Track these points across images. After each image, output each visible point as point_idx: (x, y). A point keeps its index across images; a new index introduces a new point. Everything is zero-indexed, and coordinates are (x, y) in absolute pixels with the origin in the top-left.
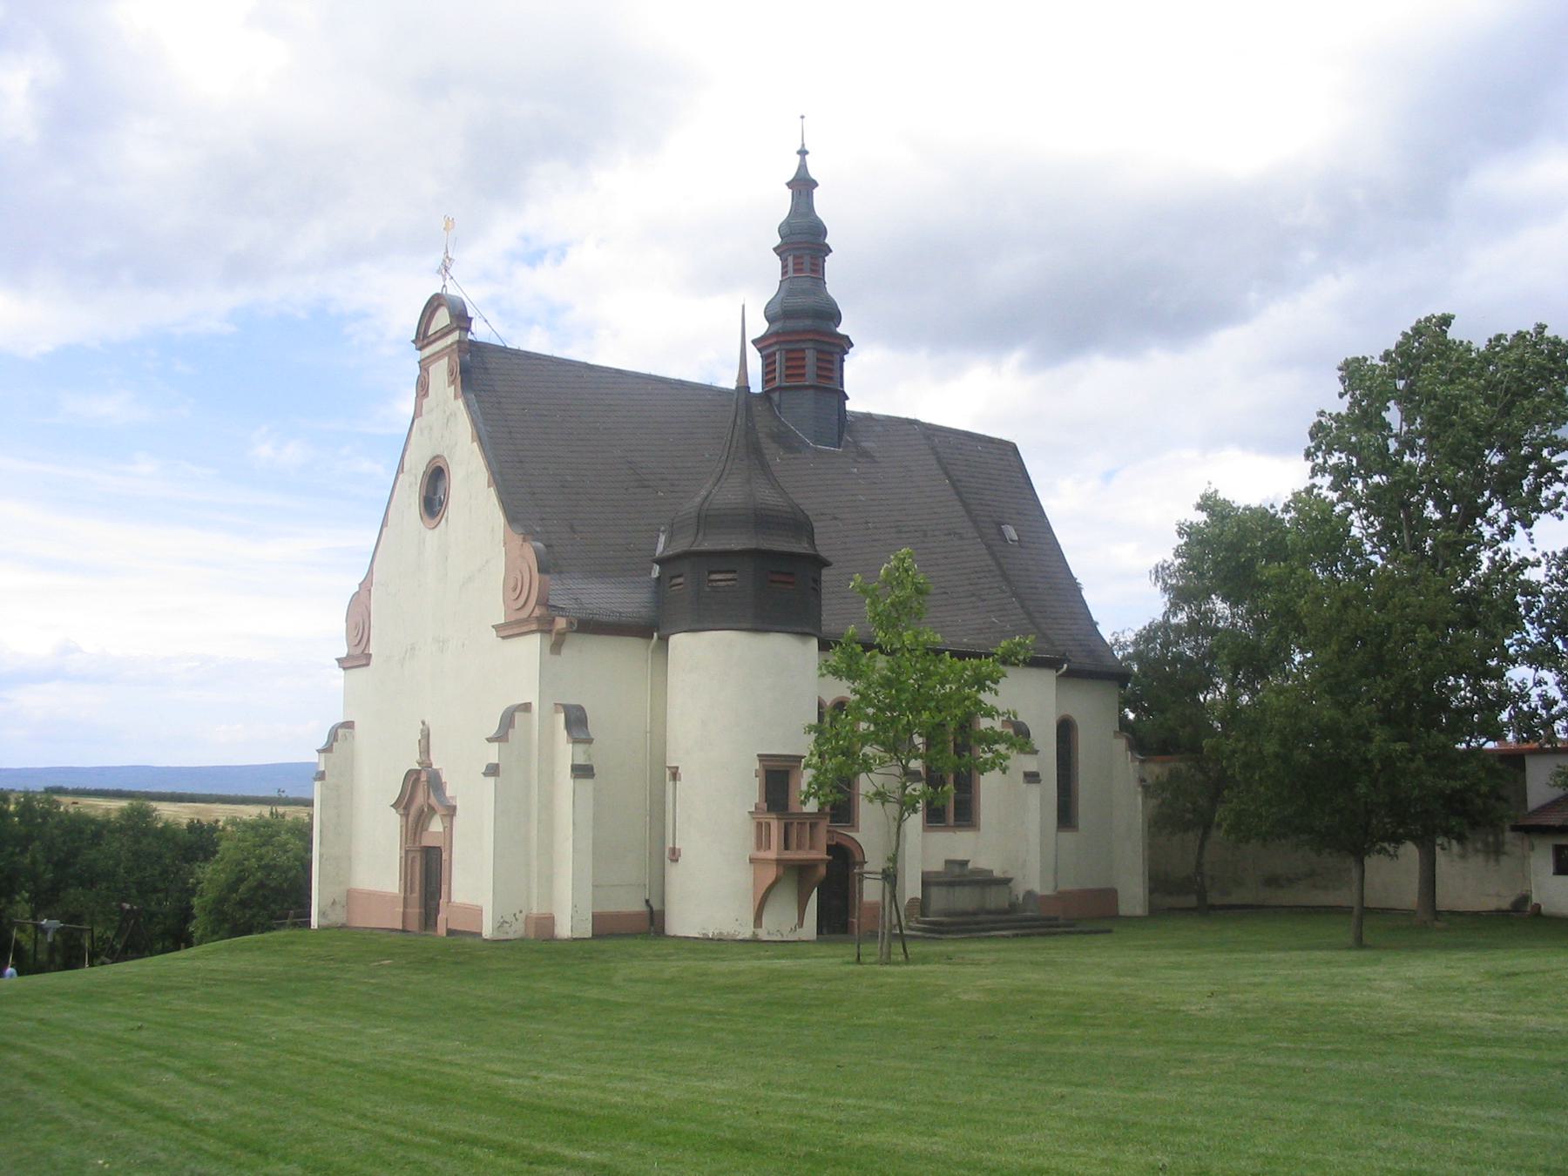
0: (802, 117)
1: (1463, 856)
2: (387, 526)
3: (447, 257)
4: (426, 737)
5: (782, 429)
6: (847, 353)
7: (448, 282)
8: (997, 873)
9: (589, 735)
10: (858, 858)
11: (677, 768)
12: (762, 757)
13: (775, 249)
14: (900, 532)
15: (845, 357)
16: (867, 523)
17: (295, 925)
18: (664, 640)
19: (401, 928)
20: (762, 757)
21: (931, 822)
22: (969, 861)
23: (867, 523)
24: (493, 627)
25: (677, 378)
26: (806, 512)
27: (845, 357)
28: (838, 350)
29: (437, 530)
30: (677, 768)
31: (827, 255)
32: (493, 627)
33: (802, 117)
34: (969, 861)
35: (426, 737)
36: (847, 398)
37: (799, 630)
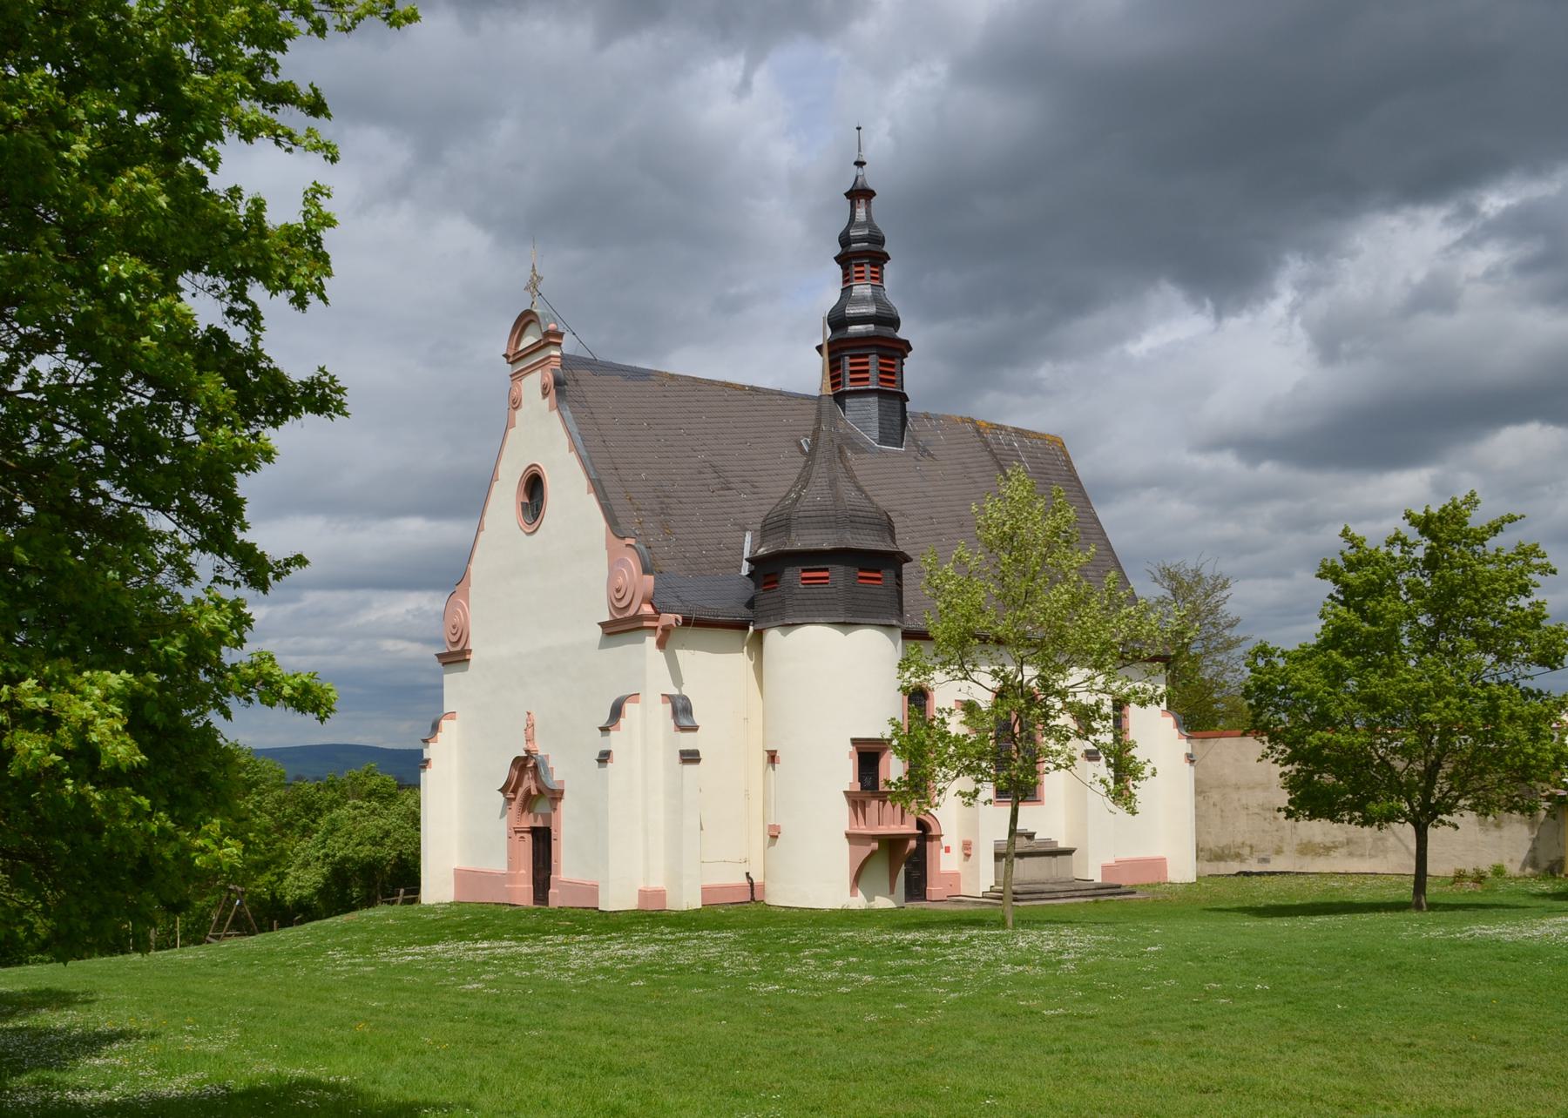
0: (859, 129)
1: (1498, 826)
2: (483, 530)
3: (535, 274)
4: (530, 726)
5: (848, 431)
6: (906, 356)
7: (537, 300)
8: (1062, 845)
9: (694, 722)
10: (934, 832)
11: (776, 751)
12: (855, 741)
13: (836, 258)
14: (962, 526)
15: (905, 360)
16: (932, 518)
17: (405, 902)
18: (759, 635)
19: (1019, 827)
20: (855, 741)
21: (1000, 797)
22: (1034, 833)
23: (932, 518)
24: (599, 624)
25: (722, 380)
26: (1548, 669)
27: (905, 360)
28: (899, 354)
29: (531, 537)
30: (776, 751)
31: (885, 262)
32: (599, 624)
33: (859, 129)
34: (1034, 833)
35: (530, 726)
36: (908, 400)
37: (877, 621)
